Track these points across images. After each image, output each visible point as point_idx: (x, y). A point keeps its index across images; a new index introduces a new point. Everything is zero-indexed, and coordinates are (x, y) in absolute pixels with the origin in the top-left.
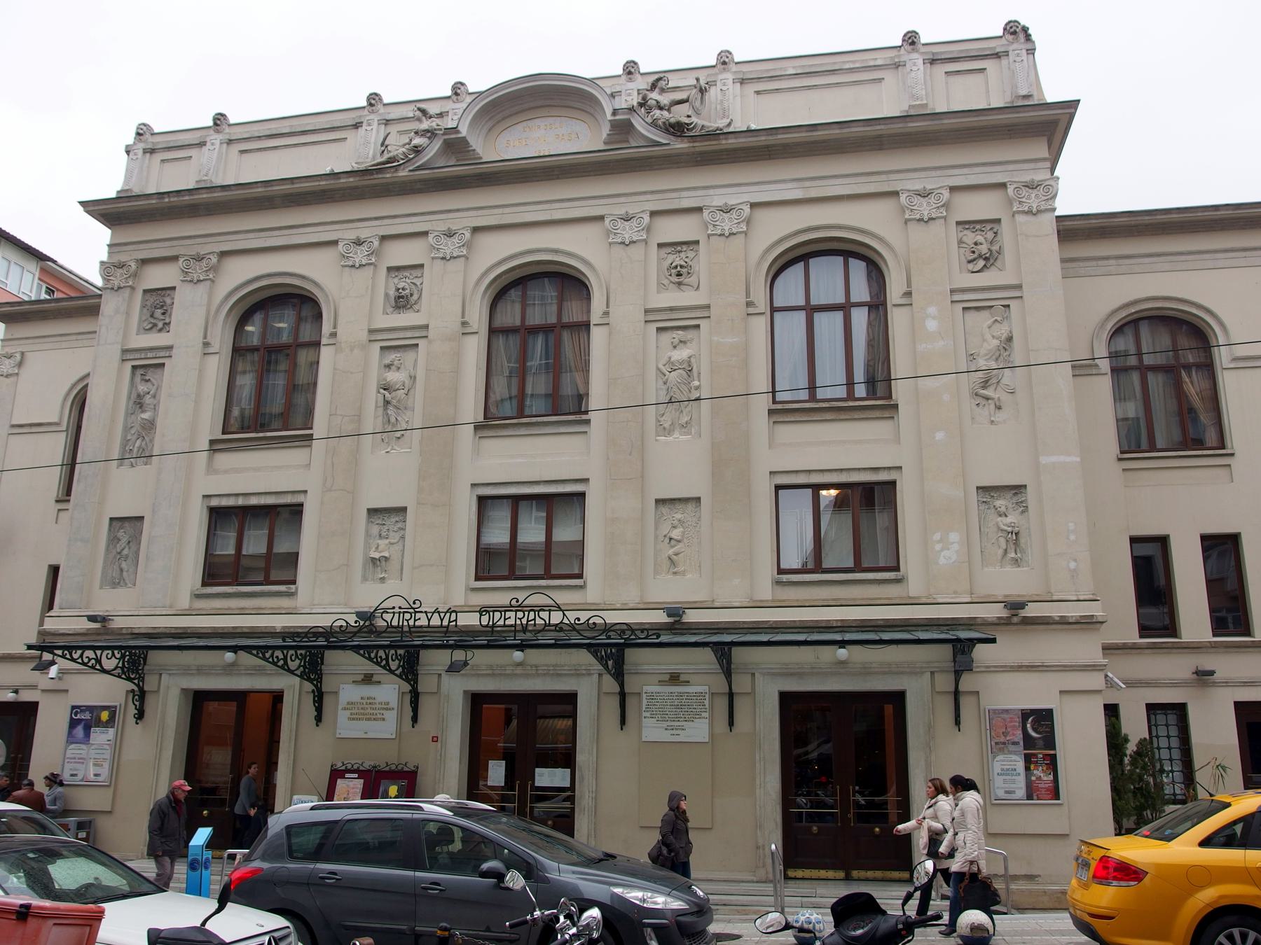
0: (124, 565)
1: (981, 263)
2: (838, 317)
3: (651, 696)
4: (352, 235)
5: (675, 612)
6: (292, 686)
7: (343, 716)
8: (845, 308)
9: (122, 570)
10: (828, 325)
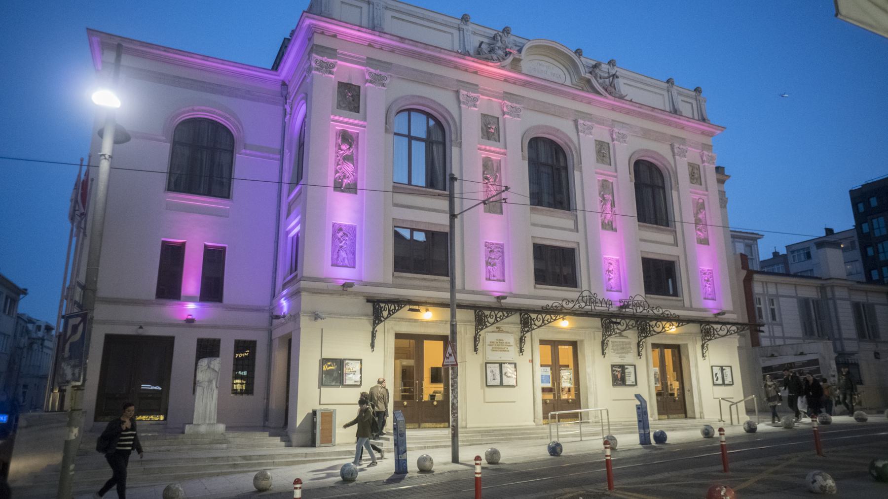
7: (489, 349)
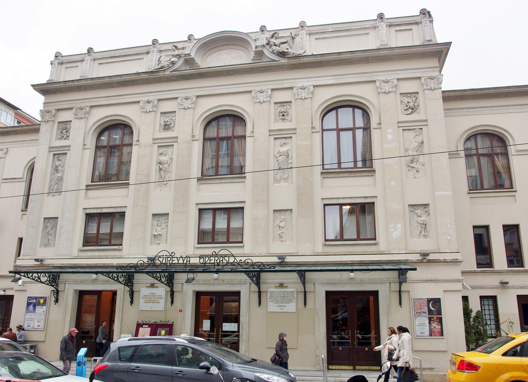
0: (50, 238)
1: (410, 111)
2: (350, 133)
3: (272, 293)
4: (146, 99)
5: (281, 257)
6: (121, 289)
8: (353, 129)
9: (49, 240)
10: (346, 137)
